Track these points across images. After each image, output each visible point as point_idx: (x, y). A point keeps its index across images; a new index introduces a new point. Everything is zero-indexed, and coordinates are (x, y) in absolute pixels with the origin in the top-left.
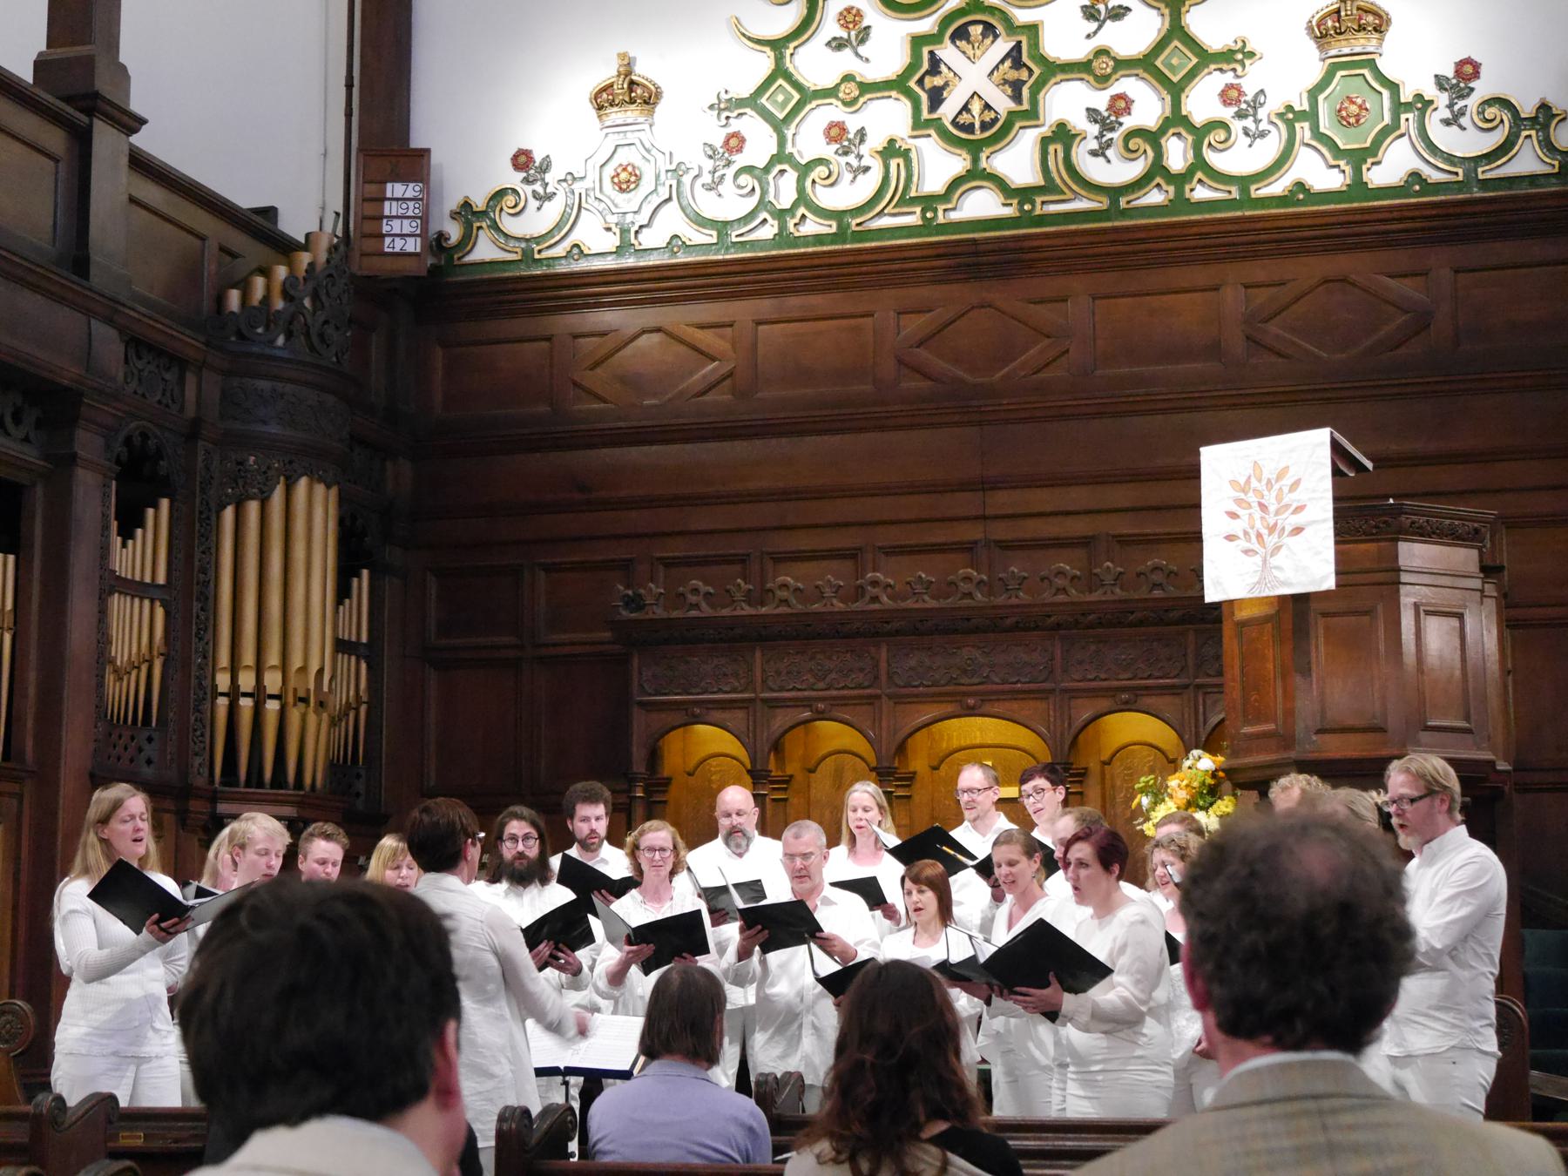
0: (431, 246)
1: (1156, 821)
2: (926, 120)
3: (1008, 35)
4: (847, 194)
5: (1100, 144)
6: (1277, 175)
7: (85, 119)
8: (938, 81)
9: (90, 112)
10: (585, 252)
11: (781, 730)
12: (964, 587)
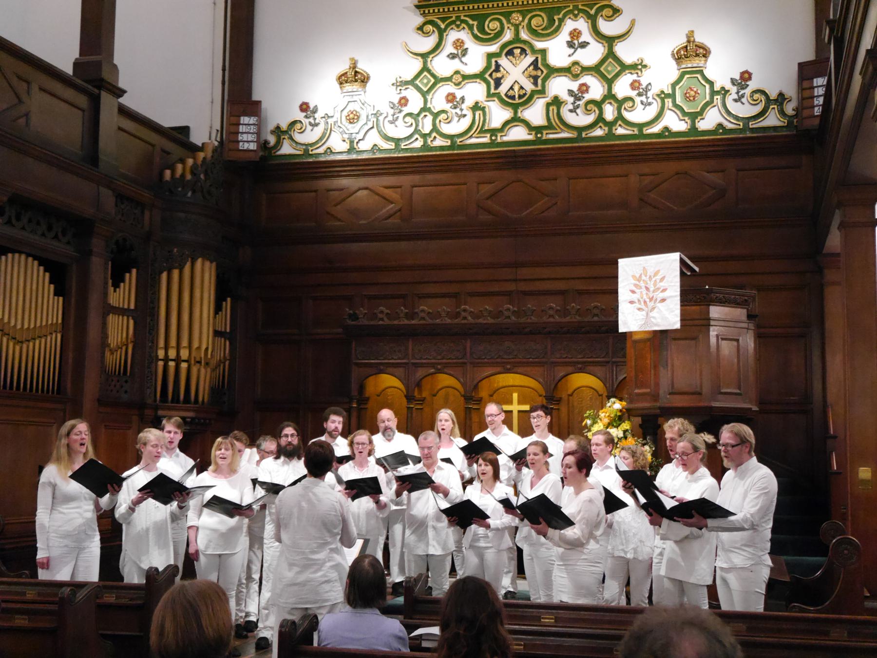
0: (261, 147)
1: (593, 432)
2: (493, 93)
3: (532, 54)
4: (456, 127)
5: (574, 106)
6: (656, 123)
7: (96, 91)
8: (499, 75)
9: (99, 88)
10: (333, 151)
11: (421, 377)
12: (506, 314)
